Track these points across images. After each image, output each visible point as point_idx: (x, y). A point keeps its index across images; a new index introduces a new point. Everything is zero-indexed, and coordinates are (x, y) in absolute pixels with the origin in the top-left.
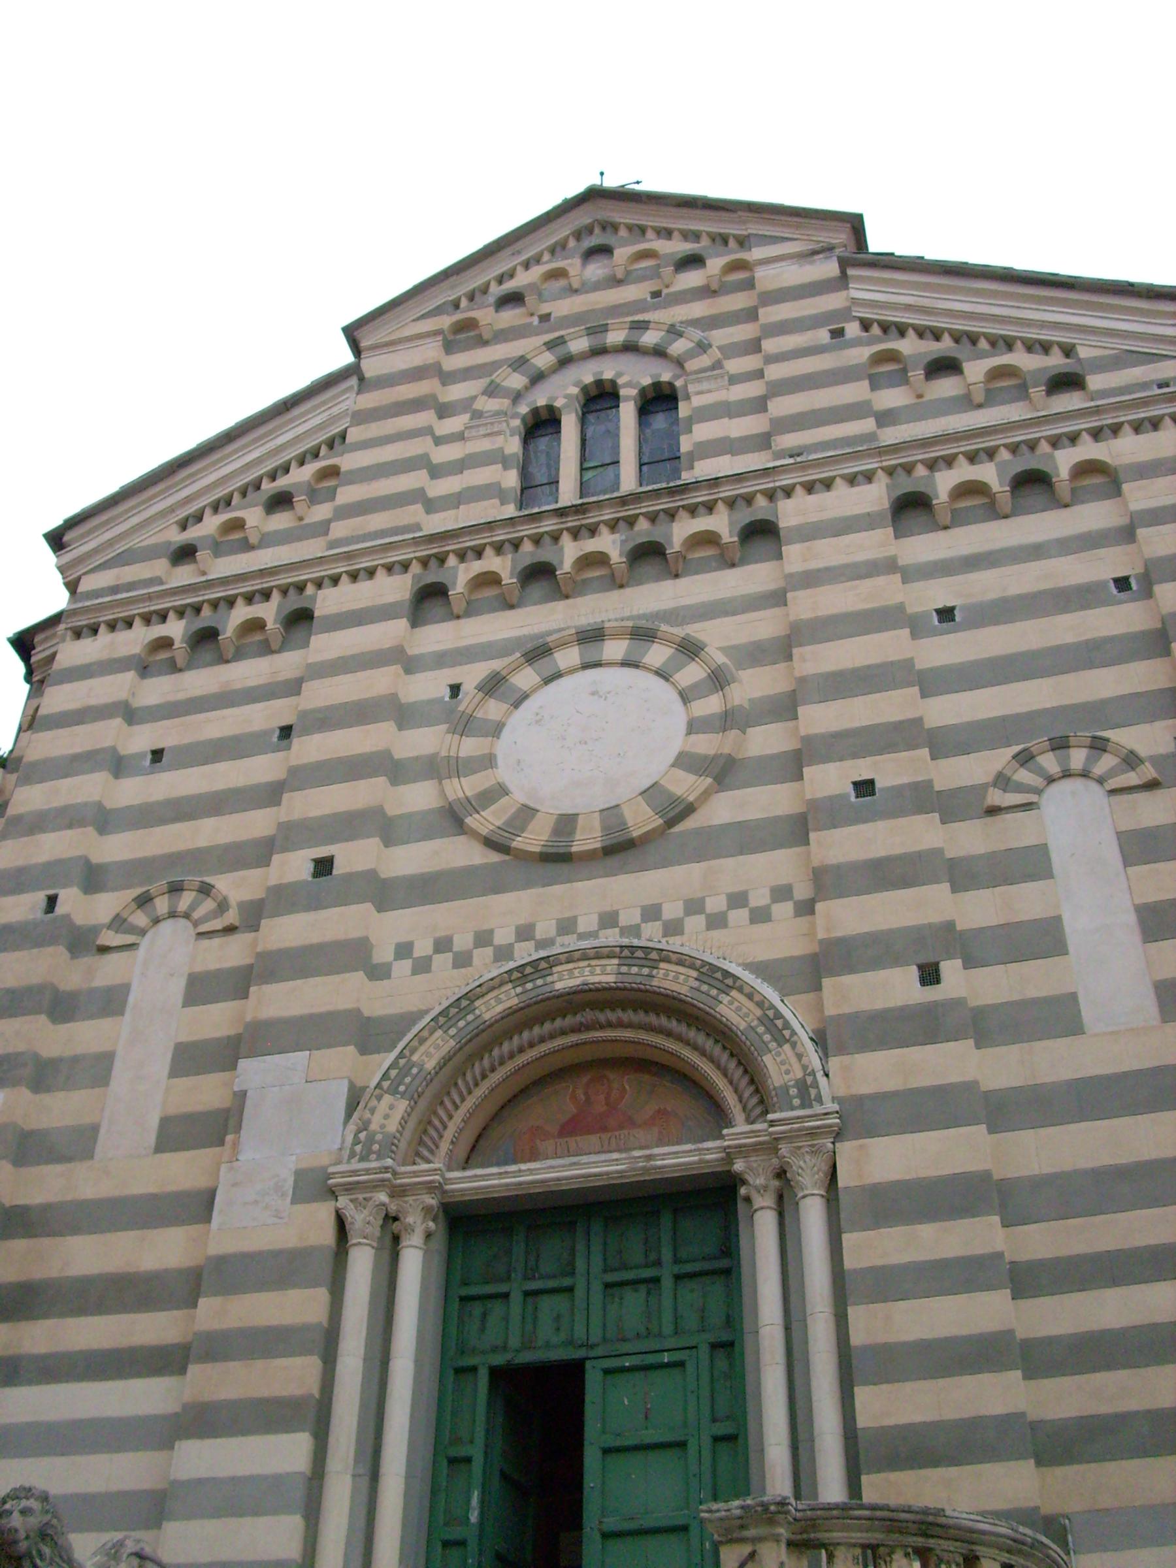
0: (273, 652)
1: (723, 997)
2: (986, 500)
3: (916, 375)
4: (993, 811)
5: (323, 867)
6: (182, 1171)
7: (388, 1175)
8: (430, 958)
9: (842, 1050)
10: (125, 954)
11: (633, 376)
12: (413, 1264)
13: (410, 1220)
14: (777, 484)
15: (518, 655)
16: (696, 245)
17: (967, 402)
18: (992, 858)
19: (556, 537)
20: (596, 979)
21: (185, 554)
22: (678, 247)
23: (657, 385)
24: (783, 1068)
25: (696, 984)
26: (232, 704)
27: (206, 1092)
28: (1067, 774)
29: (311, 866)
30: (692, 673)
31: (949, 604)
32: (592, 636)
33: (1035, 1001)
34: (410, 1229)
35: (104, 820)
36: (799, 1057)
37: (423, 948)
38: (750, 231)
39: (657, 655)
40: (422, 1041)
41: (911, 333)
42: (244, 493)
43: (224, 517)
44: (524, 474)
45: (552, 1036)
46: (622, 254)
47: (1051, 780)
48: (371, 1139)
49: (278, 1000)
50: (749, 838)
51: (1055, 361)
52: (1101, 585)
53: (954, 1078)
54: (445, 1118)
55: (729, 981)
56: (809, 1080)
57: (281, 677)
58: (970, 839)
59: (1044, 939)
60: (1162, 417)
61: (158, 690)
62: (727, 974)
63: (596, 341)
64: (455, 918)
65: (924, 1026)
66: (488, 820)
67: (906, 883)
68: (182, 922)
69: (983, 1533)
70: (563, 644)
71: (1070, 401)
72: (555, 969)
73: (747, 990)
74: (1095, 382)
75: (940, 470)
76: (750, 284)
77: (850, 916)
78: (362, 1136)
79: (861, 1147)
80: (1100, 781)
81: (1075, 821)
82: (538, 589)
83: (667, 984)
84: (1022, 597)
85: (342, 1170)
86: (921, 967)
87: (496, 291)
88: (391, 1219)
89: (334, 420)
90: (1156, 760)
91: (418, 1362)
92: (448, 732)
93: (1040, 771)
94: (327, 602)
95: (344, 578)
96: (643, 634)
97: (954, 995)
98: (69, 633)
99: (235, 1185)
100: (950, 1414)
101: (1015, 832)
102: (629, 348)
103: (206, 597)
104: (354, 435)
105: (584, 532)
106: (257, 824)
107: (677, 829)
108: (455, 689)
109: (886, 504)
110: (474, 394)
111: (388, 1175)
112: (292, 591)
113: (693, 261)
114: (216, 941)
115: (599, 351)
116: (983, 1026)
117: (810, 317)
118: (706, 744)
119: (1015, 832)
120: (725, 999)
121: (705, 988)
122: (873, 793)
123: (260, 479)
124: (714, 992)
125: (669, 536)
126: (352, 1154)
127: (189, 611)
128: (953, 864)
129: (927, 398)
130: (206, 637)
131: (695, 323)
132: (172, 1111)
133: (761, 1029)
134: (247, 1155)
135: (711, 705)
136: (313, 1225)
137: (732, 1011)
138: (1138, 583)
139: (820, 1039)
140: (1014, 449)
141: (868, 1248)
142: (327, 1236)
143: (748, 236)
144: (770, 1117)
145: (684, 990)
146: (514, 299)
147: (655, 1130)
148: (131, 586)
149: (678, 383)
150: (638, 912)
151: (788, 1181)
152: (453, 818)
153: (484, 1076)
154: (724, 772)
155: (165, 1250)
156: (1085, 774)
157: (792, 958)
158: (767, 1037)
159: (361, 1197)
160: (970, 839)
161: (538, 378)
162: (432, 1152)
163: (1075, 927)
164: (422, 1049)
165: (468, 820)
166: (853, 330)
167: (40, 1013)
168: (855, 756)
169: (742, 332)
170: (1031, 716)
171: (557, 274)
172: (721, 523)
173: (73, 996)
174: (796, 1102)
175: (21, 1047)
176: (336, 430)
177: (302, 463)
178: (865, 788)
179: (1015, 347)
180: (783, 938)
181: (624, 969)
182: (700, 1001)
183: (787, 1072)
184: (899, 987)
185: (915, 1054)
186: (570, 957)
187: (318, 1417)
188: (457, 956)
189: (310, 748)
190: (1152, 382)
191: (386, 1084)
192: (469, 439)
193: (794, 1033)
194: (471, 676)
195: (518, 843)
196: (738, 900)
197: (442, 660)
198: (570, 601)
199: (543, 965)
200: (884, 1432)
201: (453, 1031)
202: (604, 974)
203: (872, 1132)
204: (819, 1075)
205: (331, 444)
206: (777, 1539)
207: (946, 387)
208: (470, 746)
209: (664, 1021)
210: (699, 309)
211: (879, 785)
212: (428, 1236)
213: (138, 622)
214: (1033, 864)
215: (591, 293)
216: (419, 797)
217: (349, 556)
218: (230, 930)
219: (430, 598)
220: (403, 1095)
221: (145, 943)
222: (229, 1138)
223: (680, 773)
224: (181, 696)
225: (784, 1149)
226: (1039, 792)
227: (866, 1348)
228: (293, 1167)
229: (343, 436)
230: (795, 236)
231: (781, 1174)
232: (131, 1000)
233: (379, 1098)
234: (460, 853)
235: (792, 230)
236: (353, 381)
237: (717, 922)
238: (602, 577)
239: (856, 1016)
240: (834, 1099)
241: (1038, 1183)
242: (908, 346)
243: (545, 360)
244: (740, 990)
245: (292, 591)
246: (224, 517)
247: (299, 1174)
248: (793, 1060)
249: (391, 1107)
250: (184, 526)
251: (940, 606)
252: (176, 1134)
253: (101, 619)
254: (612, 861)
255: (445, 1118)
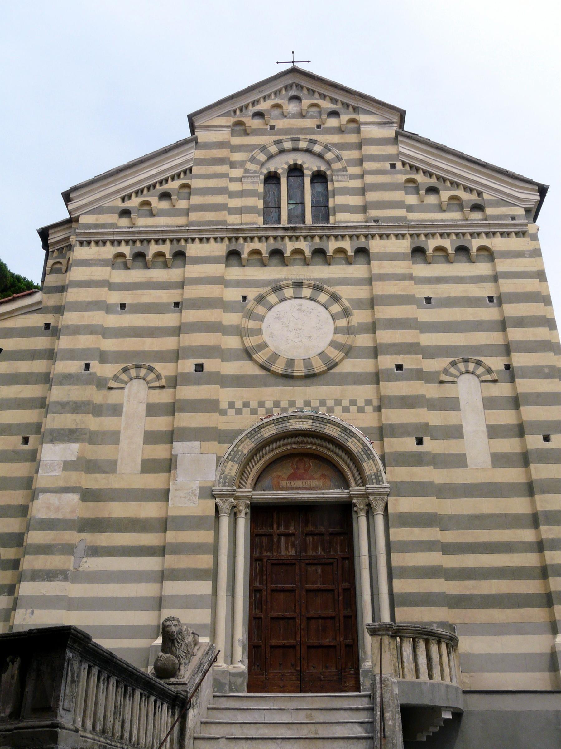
0: (168, 268)
1: (349, 439)
2: (444, 254)
3: (422, 192)
4: (442, 382)
5: (199, 368)
6: (155, 481)
7: (234, 493)
8: (242, 409)
9: (390, 465)
10: (119, 392)
11: (311, 165)
12: (243, 524)
13: (241, 508)
14: (370, 233)
15: (269, 288)
16: (335, 106)
17: (440, 208)
18: (440, 400)
19: (283, 238)
20: (304, 427)
21: (125, 213)
22: (327, 105)
23: (319, 171)
24: (370, 468)
25: (340, 433)
26: (153, 288)
27: (160, 452)
28: (467, 372)
29: (194, 366)
30: (336, 308)
31: (430, 296)
32: (298, 285)
33: (452, 454)
34: (240, 511)
35: (105, 332)
36: (376, 465)
37: (239, 405)
38: (359, 106)
39: (323, 297)
40: (242, 442)
41: (421, 171)
42: (149, 188)
43: (140, 199)
44: (265, 203)
45: (287, 444)
46: (306, 102)
47: (462, 373)
48: (225, 478)
49: (185, 420)
50: (357, 379)
51: (474, 198)
52: (483, 298)
53: (427, 479)
54: (249, 470)
55: (352, 434)
56: (379, 474)
57: (172, 280)
58: (431, 391)
59: (455, 432)
60: (511, 232)
61: (119, 276)
62: (351, 431)
63: (295, 145)
64: (251, 394)
65: (417, 460)
66: (261, 356)
67: (412, 406)
68: (142, 381)
69: (443, 635)
70: (287, 286)
71: (476, 216)
72: (290, 421)
73: (358, 438)
74: (489, 211)
75: (429, 239)
76: (358, 131)
77: (393, 416)
78: (222, 476)
79: (396, 500)
80: (478, 377)
81: (468, 390)
82: (275, 260)
83: (329, 432)
84: (455, 298)
85: (217, 490)
86: (417, 438)
87: (252, 110)
88: (234, 507)
89: (187, 161)
90: (498, 372)
91: (245, 557)
92: (243, 317)
93: (458, 370)
94: (193, 250)
95: (197, 240)
96: (317, 288)
97: (427, 450)
98: (78, 243)
99: (176, 490)
100: (422, 591)
101: (447, 391)
102: (308, 151)
103: (138, 238)
104: (195, 170)
105: (294, 238)
106: (169, 343)
107: (332, 371)
108: (244, 298)
109: (410, 250)
110: (244, 159)
111: (234, 493)
112: (175, 241)
113: (334, 114)
114: (157, 391)
115: (296, 150)
116: (436, 461)
117: (383, 155)
118: (341, 338)
119: (447, 391)
120: (350, 440)
121: (343, 435)
122: (402, 370)
123: (156, 183)
124: (346, 437)
125: (328, 247)
126: (219, 483)
127: (131, 242)
128: (428, 400)
129: (425, 203)
130: (140, 256)
131: (335, 145)
132: (147, 457)
133: (362, 453)
134: (180, 479)
135: (343, 323)
136: (207, 507)
137: (352, 445)
138: (497, 300)
139: (383, 458)
140: (457, 234)
141: (399, 534)
142: (213, 512)
143: (358, 107)
144: (367, 486)
145: (336, 435)
146: (259, 115)
147: (321, 481)
148: (103, 226)
149: (328, 173)
150: (318, 402)
151: (371, 508)
152: (248, 354)
153: (263, 457)
154: (348, 351)
155: (150, 511)
156: (473, 373)
157: (372, 427)
158: (364, 456)
159: (224, 499)
160: (431, 391)
161: (271, 157)
162: (246, 483)
163: (467, 429)
164: (242, 445)
165: (254, 356)
166: (399, 165)
167: (89, 413)
168: (396, 354)
169: (354, 154)
170: (456, 347)
171: (277, 106)
172: (347, 245)
173: (101, 406)
174: (374, 481)
175: (83, 426)
176: (188, 166)
177: (173, 179)
178: (399, 367)
179: (460, 187)
180: (369, 419)
181: (314, 424)
182: (342, 440)
183: (371, 470)
184: (408, 444)
185: (415, 469)
186: (295, 417)
187: (212, 575)
188: (252, 409)
189: (190, 316)
190: (509, 215)
191: (230, 457)
192: (245, 182)
193: (374, 456)
194: (252, 293)
195: (273, 368)
196: (353, 402)
197: (238, 284)
198: (288, 267)
199: (285, 419)
200: (401, 595)
201: (253, 440)
202: (308, 425)
203: (399, 495)
204: (383, 473)
205: (185, 172)
206: (388, 635)
207: (432, 199)
208: (252, 324)
209: (327, 445)
210: (335, 138)
211: (404, 367)
212: (246, 514)
213: (108, 243)
214: (453, 404)
215: (292, 119)
216: (232, 342)
217: (199, 231)
218: (162, 387)
219: (233, 255)
220: (236, 462)
221: (127, 387)
222: (172, 471)
223: (332, 349)
224: (130, 281)
225: (371, 498)
226: (457, 377)
227: (397, 567)
228: (198, 485)
229: (191, 169)
230: (377, 113)
231: (369, 505)
232: (124, 410)
233: (228, 462)
234: (248, 368)
235: (376, 110)
236: (194, 144)
237: (346, 410)
238: (300, 259)
239: (395, 453)
240: (388, 482)
241: (451, 517)
242: (420, 178)
243: (274, 149)
244: (355, 438)
245: (175, 241)
246: (140, 199)
247: (201, 488)
248: (374, 466)
249: (232, 466)
250: (123, 199)
251: (427, 296)
252: (148, 466)
253: (92, 239)
254: (309, 381)
255: (249, 470)
